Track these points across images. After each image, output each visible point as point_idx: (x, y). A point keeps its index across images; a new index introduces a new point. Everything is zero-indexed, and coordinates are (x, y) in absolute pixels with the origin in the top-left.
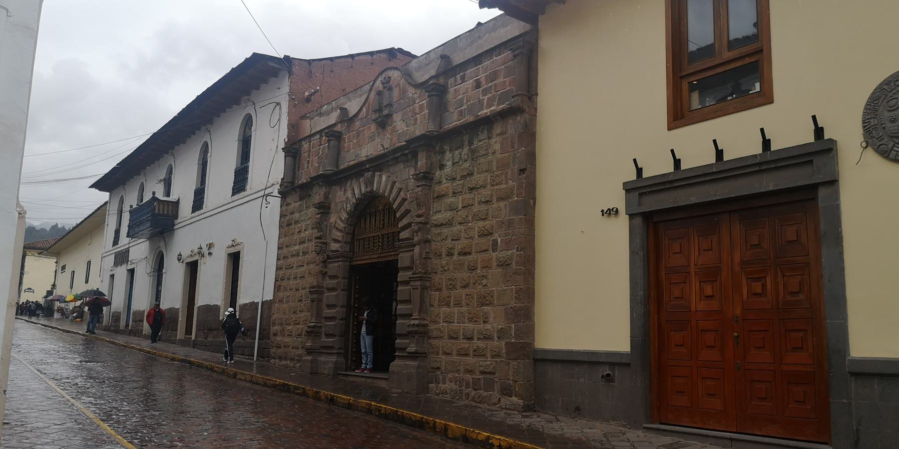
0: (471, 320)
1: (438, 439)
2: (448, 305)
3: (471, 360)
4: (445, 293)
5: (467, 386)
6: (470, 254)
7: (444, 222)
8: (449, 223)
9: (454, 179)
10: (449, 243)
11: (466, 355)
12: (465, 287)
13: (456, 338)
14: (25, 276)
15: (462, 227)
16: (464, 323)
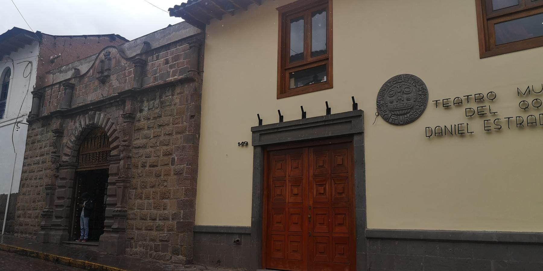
0: (155, 208)
2: (141, 198)
3: (154, 233)
4: (139, 190)
5: (151, 250)
6: (157, 166)
7: (141, 146)
8: (144, 147)
9: (149, 119)
10: (143, 159)
12: (152, 187)
15: (153, 150)
16: (151, 210)
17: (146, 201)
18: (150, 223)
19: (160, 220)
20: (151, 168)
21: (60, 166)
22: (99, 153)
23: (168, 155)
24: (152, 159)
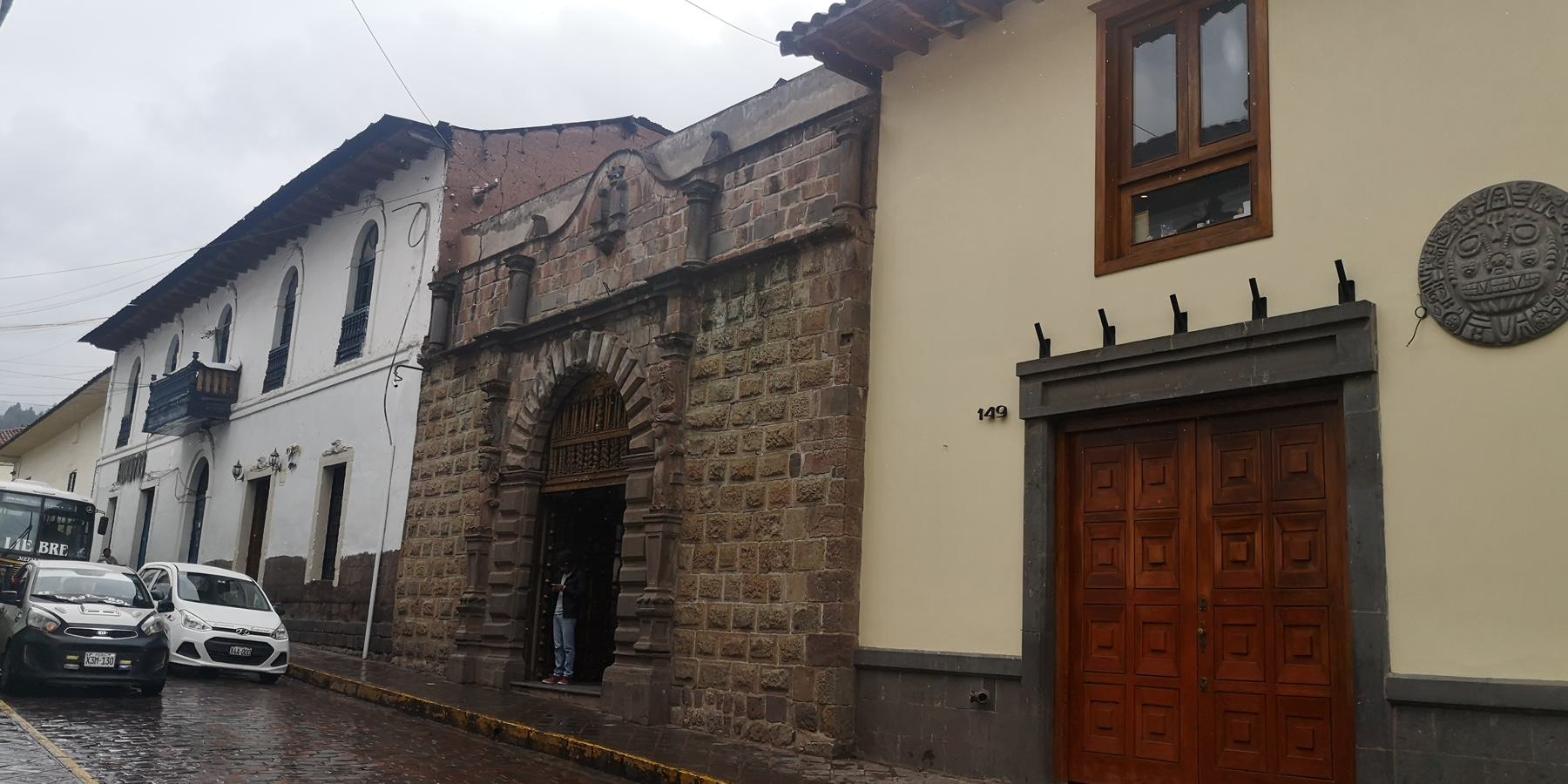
0: (748, 595)
3: (746, 666)
4: (706, 546)
5: (738, 712)
6: (751, 478)
7: (709, 422)
8: (717, 425)
9: (729, 347)
10: (715, 458)
11: (740, 656)
12: (740, 536)
13: (723, 627)
15: (739, 432)
16: (737, 600)
17: (724, 576)
18: (737, 637)
19: (762, 628)
24: (740, 459)
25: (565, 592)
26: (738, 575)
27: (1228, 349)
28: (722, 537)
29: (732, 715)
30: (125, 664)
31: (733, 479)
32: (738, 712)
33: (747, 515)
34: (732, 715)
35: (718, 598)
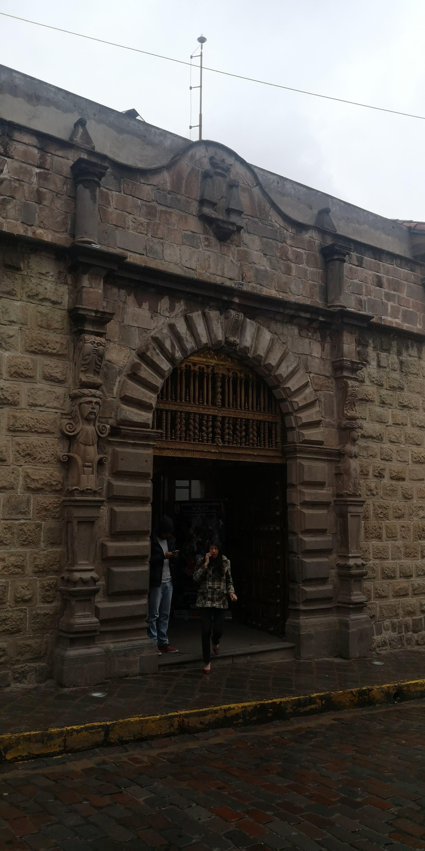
0: (407, 555)
1: (327, 719)
2: (379, 537)
3: (411, 601)
4: (373, 522)
5: (407, 630)
6: (403, 479)
7: (374, 435)
8: (379, 439)
9: (381, 385)
10: (378, 462)
11: (406, 595)
12: (399, 517)
13: (392, 578)
14: (199, 113)
15: (393, 447)
16: (400, 559)
17: (390, 543)
18: (402, 583)
19: (419, 576)
20: (394, 482)
21: (115, 431)
22: (224, 418)
23: (387, 460)
24: (395, 466)
25: (172, 559)
26: (400, 543)
27: (88, 504)
28: (386, 517)
29: (404, 634)
30: (235, 722)
31: (392, 478)
32: (407, 630)
33: (403, 503)
34: (404, 634)
35: (387, 559)
